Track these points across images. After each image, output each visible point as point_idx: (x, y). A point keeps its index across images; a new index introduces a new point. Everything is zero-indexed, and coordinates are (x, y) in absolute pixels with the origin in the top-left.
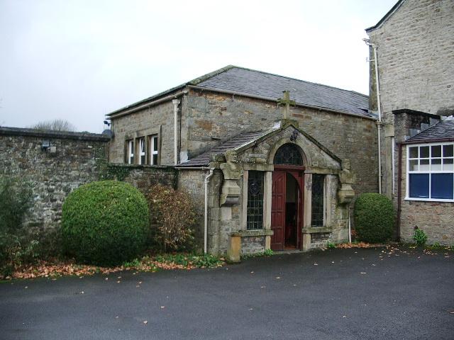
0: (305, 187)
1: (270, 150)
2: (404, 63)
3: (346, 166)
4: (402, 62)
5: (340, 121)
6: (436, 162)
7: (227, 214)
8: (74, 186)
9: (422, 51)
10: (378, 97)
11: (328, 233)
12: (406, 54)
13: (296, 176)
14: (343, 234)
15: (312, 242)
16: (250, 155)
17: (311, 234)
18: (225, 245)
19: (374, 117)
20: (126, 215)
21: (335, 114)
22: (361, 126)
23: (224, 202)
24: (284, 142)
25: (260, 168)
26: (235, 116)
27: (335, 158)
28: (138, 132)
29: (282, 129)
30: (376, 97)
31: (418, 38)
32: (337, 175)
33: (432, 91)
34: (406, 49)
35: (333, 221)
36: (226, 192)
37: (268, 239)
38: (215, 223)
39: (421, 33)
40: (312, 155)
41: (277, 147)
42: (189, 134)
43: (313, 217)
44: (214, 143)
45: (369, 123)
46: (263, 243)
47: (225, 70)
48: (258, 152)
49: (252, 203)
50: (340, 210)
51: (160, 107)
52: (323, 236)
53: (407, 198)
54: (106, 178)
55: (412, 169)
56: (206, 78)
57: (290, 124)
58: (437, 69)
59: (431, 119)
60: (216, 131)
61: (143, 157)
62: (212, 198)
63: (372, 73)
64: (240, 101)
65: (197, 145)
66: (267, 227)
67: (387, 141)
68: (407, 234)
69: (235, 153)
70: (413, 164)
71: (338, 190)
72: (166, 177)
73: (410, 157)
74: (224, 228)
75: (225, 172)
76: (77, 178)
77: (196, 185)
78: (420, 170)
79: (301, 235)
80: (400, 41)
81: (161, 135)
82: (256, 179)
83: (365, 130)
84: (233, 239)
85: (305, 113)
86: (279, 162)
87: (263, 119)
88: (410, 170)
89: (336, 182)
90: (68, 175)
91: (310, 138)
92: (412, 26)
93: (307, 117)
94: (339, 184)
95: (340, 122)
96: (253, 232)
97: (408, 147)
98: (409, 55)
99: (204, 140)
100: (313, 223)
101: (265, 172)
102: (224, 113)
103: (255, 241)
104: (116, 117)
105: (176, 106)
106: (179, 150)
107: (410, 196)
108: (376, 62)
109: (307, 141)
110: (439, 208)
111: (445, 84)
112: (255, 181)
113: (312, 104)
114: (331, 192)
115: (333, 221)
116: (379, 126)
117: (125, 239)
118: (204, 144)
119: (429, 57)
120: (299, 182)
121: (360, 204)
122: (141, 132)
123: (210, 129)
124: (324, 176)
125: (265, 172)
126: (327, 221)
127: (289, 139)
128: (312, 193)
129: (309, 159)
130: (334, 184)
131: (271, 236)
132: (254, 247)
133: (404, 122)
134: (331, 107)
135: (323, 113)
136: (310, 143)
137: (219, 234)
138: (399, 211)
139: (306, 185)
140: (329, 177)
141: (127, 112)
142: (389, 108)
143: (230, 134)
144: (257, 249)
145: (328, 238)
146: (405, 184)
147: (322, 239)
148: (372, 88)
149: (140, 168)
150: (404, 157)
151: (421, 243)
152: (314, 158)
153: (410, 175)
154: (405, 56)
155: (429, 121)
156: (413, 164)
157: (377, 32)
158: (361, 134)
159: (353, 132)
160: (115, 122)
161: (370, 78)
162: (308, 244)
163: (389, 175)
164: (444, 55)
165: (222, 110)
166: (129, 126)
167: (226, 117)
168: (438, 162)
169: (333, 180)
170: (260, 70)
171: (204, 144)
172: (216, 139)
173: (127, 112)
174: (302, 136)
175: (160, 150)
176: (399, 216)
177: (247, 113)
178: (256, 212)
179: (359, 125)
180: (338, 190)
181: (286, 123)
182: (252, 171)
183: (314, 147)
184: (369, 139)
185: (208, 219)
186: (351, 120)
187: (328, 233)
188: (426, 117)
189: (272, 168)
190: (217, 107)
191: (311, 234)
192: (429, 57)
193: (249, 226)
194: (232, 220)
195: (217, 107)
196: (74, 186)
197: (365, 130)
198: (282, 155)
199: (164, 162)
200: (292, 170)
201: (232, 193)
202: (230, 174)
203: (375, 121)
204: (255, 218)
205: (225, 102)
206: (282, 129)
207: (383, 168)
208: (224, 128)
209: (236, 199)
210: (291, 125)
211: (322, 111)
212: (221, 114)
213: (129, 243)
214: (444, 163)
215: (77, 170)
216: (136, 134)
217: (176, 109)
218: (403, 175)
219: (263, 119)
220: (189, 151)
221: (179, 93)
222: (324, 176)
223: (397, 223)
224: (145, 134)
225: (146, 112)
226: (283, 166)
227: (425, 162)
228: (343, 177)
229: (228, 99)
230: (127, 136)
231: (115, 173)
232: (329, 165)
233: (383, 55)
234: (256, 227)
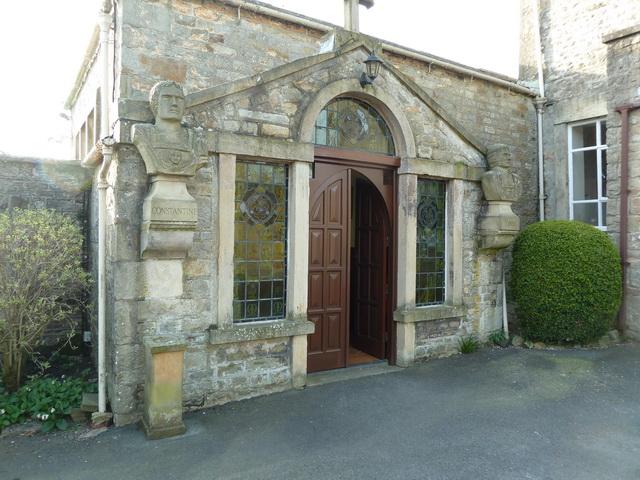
0: (400, 208)
11: (457, 319)
14: (491, 317)
15: (418, 344)
16: (243, 113)
17: (416, 323)
21: (460, 75)
23: (144, 248)
24: (344, 87)
32: (479, 183)
37: (300, 348)
40: (416, 131)
43: (421, 281)
46: (285, 355)
52: (444, 325)
57: (358, 44)
64: (256, 27)
66: (296, 312)
67: (557, 132)
89: (475, 196)
94: (484, 202)
95: (470, 95)
100: (421, 297)
102: (218, 48)
109: (404, 93)
114: (464, 222)
115: (467, 291)
124: (443, 183)
126: (454, 290)
127: (356, 82)
131: (310, 337)
132: (259, 371)
135: (439, 73)
136: (412, 100)
138: (624, 264)
139: (402, 203)
140: (459, 187)
145: (456, 329)
147: (440, 332)
158: (508, 120)
159: (493, 116)
162: (409, 343)
163: (563, 195)
167: (222, 57)
169: (467, 194)
174: (391, 79)
177: (273, 54)
183: (423, 113)
184: (522, 130)
186: (490, 91)
187: (457, 319)
190: (198, 32)
191: (416, 323)
201: (164, 217)
203: (533, 97)
207: (549, 184)
210: (363, 47)
212: (211, 50)
228: (493, 187)
234: (265, 312)
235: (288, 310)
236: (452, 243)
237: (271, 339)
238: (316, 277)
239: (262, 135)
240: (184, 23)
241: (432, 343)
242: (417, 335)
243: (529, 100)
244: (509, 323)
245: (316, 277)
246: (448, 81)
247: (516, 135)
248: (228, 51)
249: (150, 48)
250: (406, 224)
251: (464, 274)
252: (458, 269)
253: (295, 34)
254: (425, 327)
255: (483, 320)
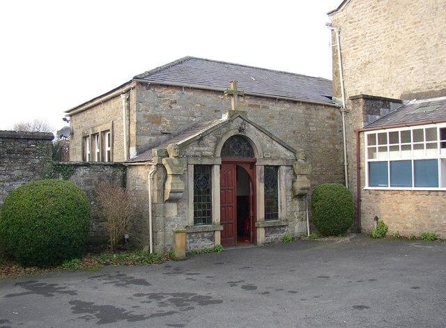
1: (217, 143)
2: (367, 46)
3: (300, 156)
4: (364, 45)
5: (300, 109)
6: (405, 148)
7: (173, 210)
8: (17, 185)
9: (384, 32)
10: (342, 84)
12: (369, 36)
13: (247, 168)
16: (195, 148)
17: (265, 228)
18: (170, 242)
19: (337, 104)
20: (63, 214)
21: (295, 102)
22: (323, 113)
23: (167, 197)
24: (232, 133)
25: (206, 162)
26: (186, 109)
27: (288, 148)
28: (93, 128)
29: (230, 121)
30: (340, 83)
31: (380, 20)
33: (395, 75)
34: (369, 31)
35: (288, 214)
36: (168, 187)
37: (218, 235)
38: (160, 219)
39: (383, 14)
40: (263, 147)
41: (224, 139)
42: (137, 128)
43: (267, 210)
44: (164, 137)
45: (332, 110)
46: (212, 239)
47: (180, 62)
48: (204, 145)
49: (200, 198)
50: (296, 202)
51: (112, 101)
53: (367, 187)
54: (51, 177)
55: (371, 156)
56: (150, 74)
58: (399, 52)
59: (391, 103)
60: (166, 124)
61: (109, 152)
62: (156, 193)
63: (335, 58)
64: (191, 94)
65: (146, 140)
68: (368, 223)
69: (177, 147)
70: (372, 152)
71: (293, 182)
72: (114, 175)
73: (369, 145)
74: (169, 225)
75: (167, 167)
76: (18, 179)
77: (143, 177)
78: (381, 157)
79: (255, 229)
80: (362, 23)
81: (113, 131)
82: (203, 173)
83: (329, 118)
84: (178, 236)
85: (262, 103)
86: (229, 154)
87: (216, 111)
88: (369, 158)
89: (291, 172)
90: (11, 175)
91: (260, 129)
92: (373, 7)
93: (264, 107)
95: (301, 111)
96: (201, 227)
97: (366, 133)
98: (372, 38)
99: (153, 135)
100: (267, 217)
101: (213, 165)
103: (203, 237)
104: (75, 113)
105: (124, 101)
106: (129, 146)
107: (370, 185)
108: (338, 47)
109: (257, 132)
110: (398, 197)
111: (408, 66)
112: (202, 176)
113: (268, 93)
116: (343, 113)
117: (63, 238)
118: (154, 138)
119: (392, 39)
120: (251, 175)
121: (317, 195)
122: (95, 129)
123: (159, 123)
124: (277, 167)
125: (213, 165)
126: (282, 214)
128: (265, 185)
129: (260, 150)
130: (288, 175)
133: (361, 108)
134: (290, 95)
135: (282, 102)
136: (261, 134)
137: (164, 231)
138: (359, 201)
139: (258, 177)
140: (283, 169)
141: (81, 109)
142: (352, 92)
143: (181, 127)
144: (205, 244)
145: (284, 231)
146: (364, 173)
147: (277, 232)
148: (336, 73)
149: (87, 165)
150: (362, 144)
151: (383, 233)
152: (266, 150)
153: (369, 163)
154: (367, 39)
155: (389, 106)
156: (372, 152)
157: (339, 15)
160: (73, 117)
161: (333, 63)
162: (261, 235)
164: (406, 36)
165: (172, 103)
166: (83, 124)
168: (408, 148)
169: (287, 172)
170: (204, 57)
171: (154, 138)
172: (166, 133)
173: (81, 109)
174: (252, 127)
175: (113, 145)
176: (359, 206)
177: (199, 105)
178: (204, 206)
179: (321, 113)
180: (293, 182)
181: (233, 115)
182: (198, 165)
184: (333, 127)
185: (152, 216)
186: (312, 108)
188: (386, 102)
189: (219, 161)
190: (166, 100)
191: (265, 228)
192: (392, 39)
193: (196, 222)
194: (180, 216)
195: (166, 100)
196: (17, 185)
197: (329, 118)
198: (231, 147)
199: (116, 159)
200: (243, 163)
202: (172, 168)
203: (339, 108)
204: (202, 214)
205: (175, 95)
206: (229, 121)
208: (174, 122)
209: (180, 195)
211: (279, 100)
213: (67, 243)
214: (414, 149)
215: (20, 169)
216: (91, 130)
217: (124, 104)
218: (362, 164)
219: (216, 111)
220: (137, 146)
221: (127, 87)
222: (277, 167)
223: (357, 214)
224: (99, 130)
225: (99, 108)
226: (233, 159)
227: (383, 149)
228: (297, 167)
229: (178, 92)
230: (83, 133)
231: (60, 171)
232: (283, 156)
233: (345, 39)
234: (204, 222)
235: (213, 221)
236: (281, 192)
237: (207, 232)
238: (223, 209)
239: (203, 157)
240: (160, 97)
241: (272, 237)
242: (266, 232)
243: (337, 109)
244: (310, 227)
245: (223, 209)
246: (287, 105)
247: (330, 130)
248: (179, 107)
249: (147, 111)
250: (260, 186)
251: (287, 206)
252: (284, 203)
253: (208, 94)
254: (268, 229)
255: (296, 227)
